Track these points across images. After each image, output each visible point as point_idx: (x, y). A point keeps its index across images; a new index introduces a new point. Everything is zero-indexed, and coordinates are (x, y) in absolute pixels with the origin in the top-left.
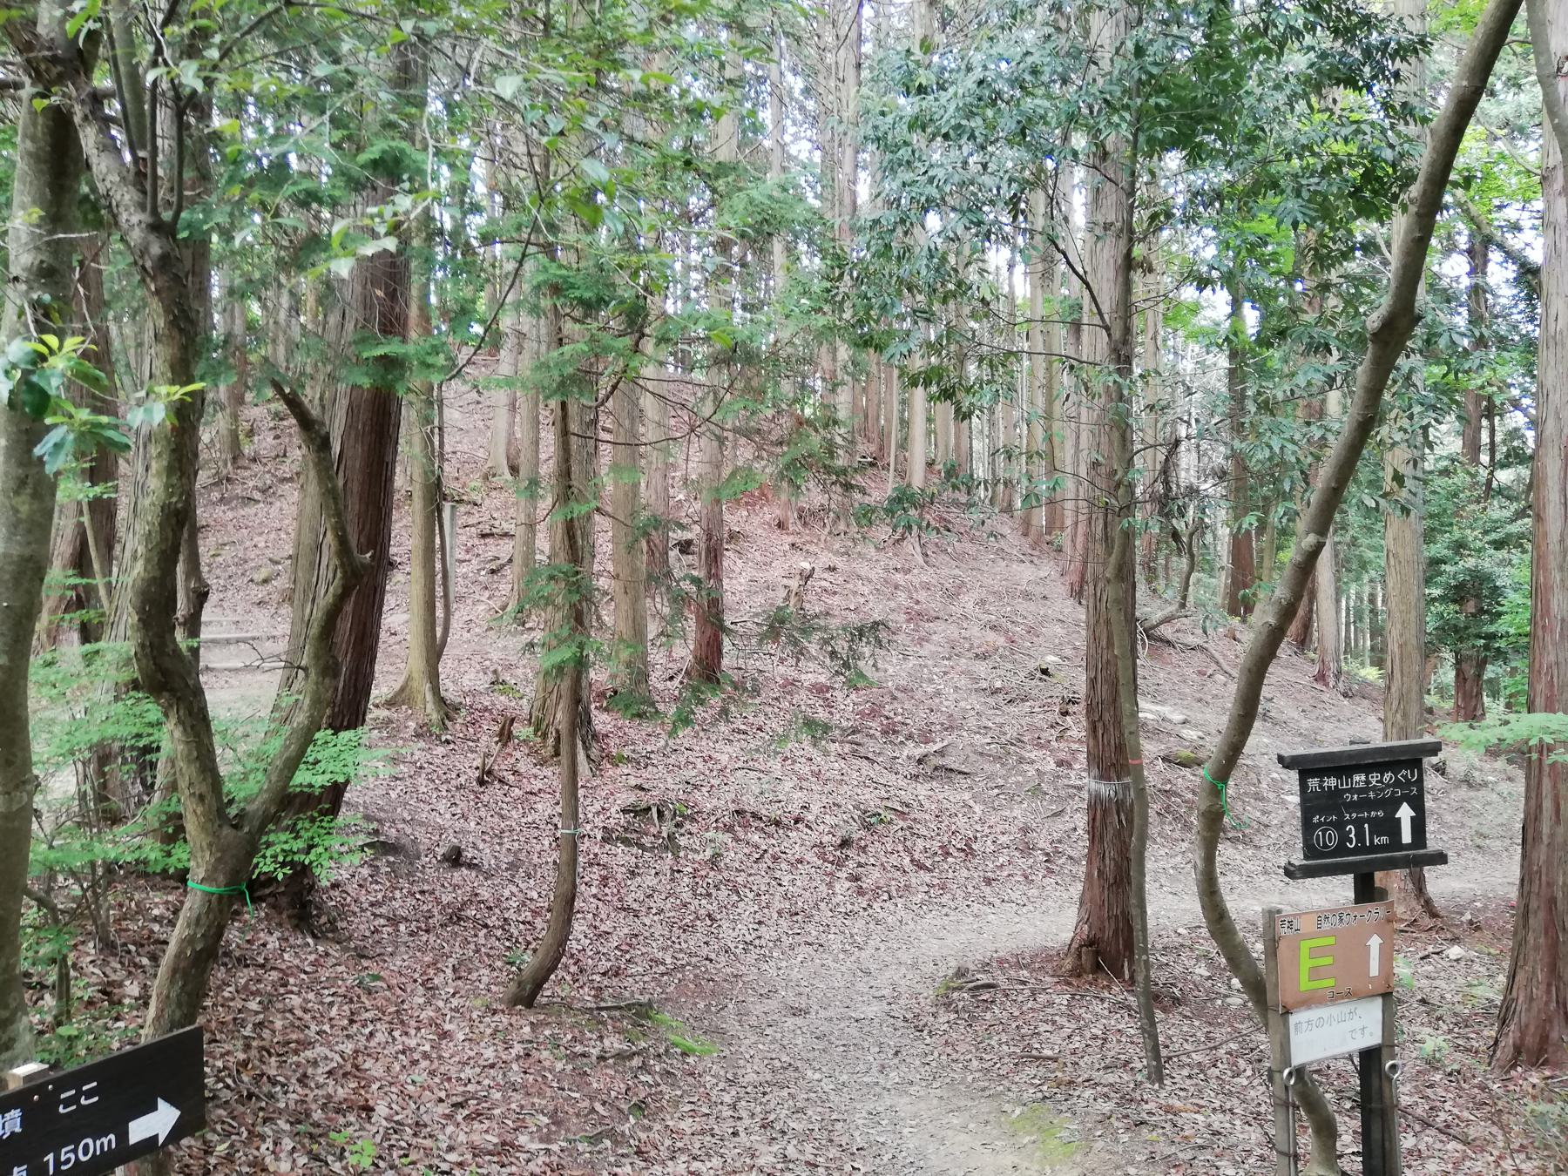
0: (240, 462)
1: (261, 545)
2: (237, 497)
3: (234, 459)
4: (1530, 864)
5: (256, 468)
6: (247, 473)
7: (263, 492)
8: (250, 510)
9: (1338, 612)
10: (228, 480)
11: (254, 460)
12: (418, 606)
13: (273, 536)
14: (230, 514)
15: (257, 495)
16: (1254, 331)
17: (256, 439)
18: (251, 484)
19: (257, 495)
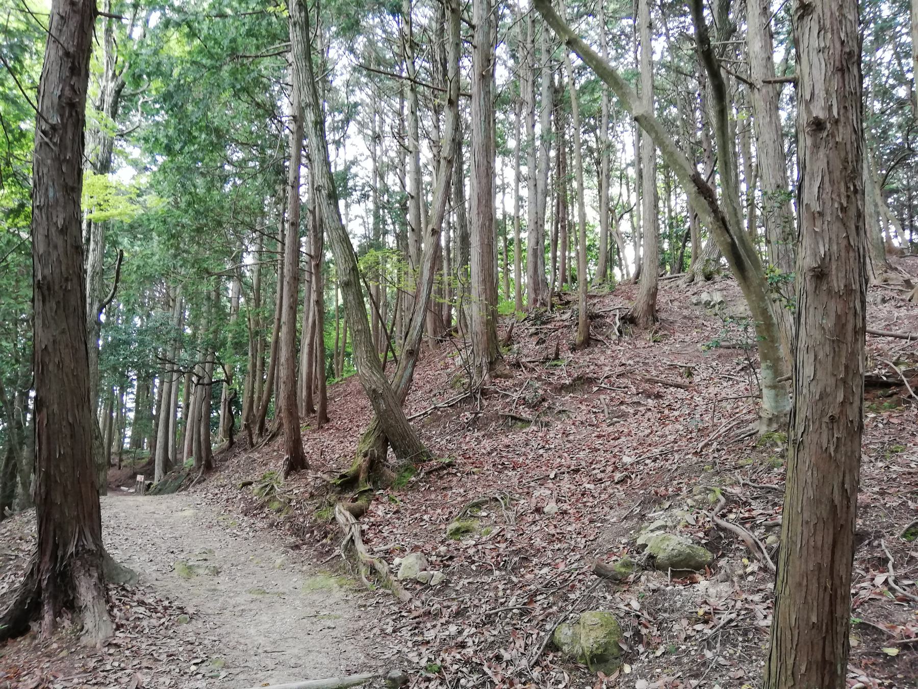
0: (500, 368)
1: (551, 507)
2: (497, 417)
3: (492, 365)
4: (82, 26)
5: (521, 375)
6: (509, 383)
7: (534, 406)
8: (517, 437)
9: (820, 64)
10: (484, 393)
11: (517, 365)
12: (821, 651)
13: (566, 485)
14: (487, 444)
15: (525, 413)
16: (332, 54)
17: (515, 347)
18: (515, 396)
19: (525, 413)
